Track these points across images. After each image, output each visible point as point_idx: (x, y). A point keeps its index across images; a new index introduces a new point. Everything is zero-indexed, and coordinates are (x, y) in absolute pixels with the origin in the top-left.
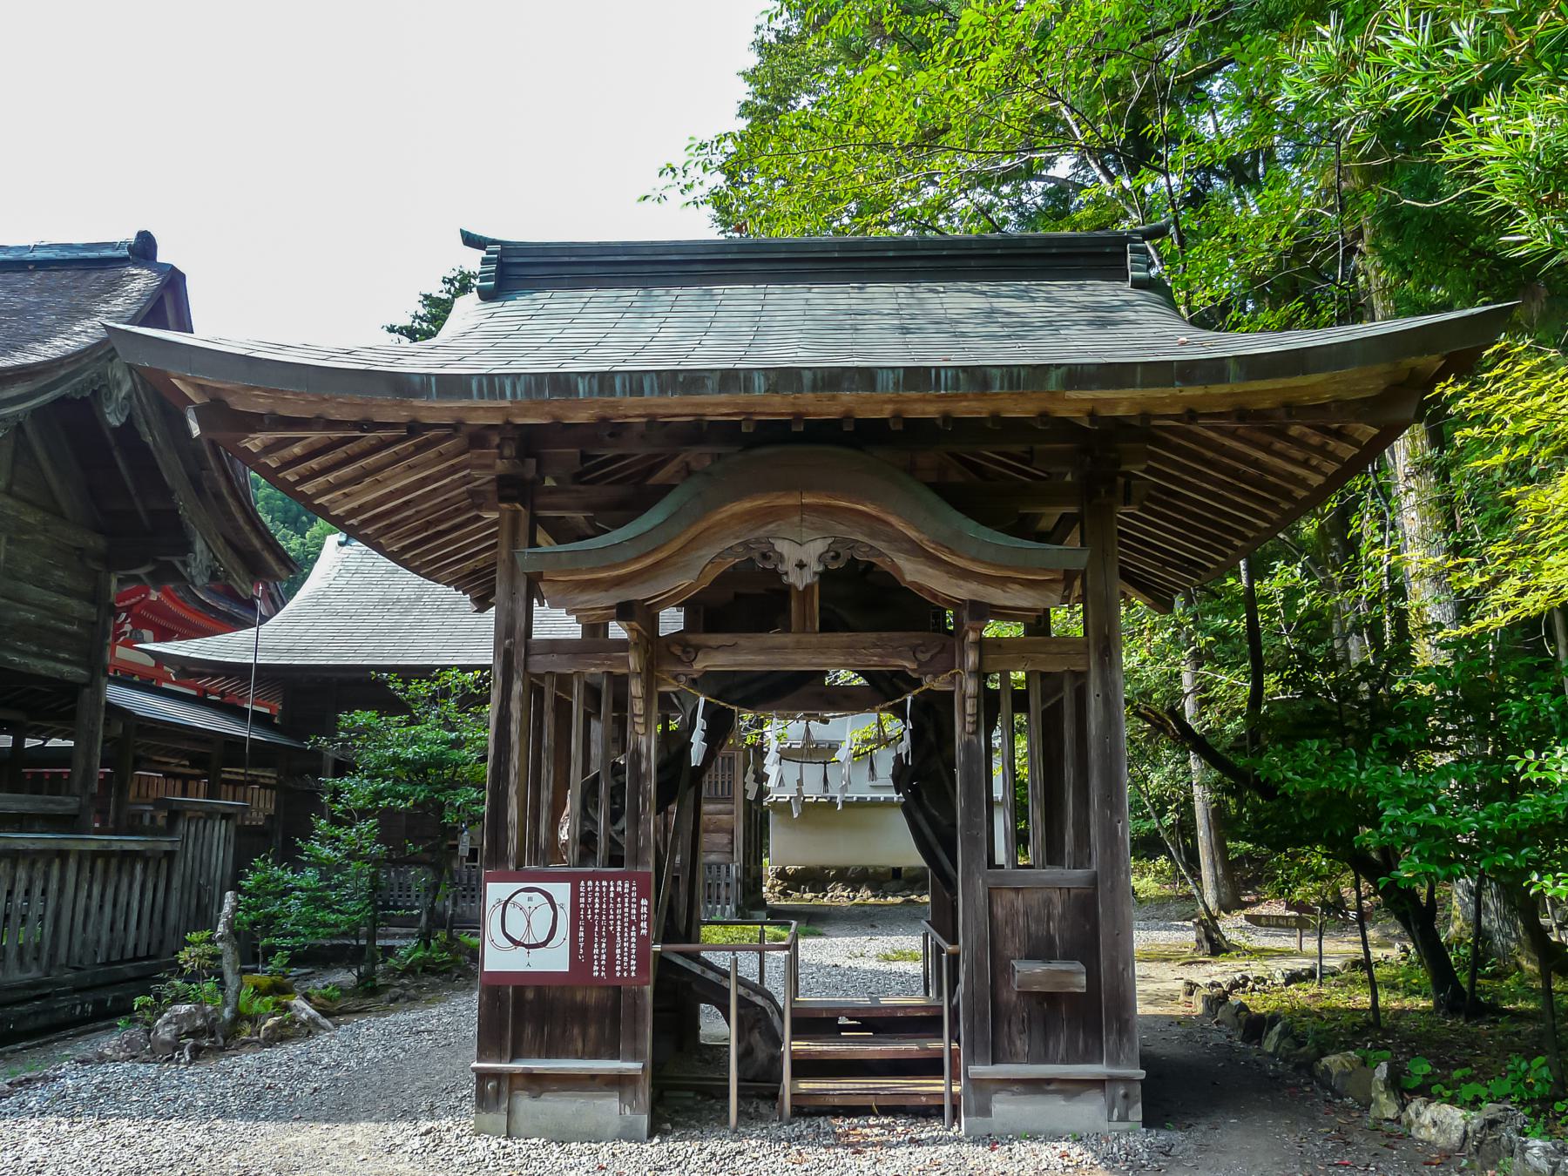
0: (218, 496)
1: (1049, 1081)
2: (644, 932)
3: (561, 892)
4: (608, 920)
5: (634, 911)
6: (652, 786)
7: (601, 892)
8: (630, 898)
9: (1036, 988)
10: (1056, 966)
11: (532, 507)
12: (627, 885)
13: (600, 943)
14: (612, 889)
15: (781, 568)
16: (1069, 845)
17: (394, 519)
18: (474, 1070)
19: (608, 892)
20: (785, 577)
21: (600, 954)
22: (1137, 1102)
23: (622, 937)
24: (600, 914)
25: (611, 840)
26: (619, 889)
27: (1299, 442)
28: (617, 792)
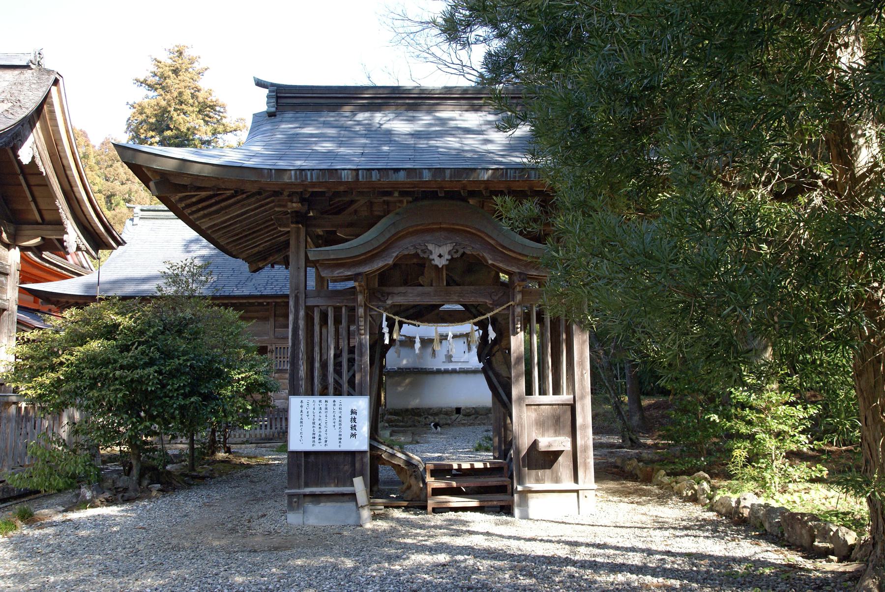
11: (307, 226)
15: (431, 257)
18: (286, 493)
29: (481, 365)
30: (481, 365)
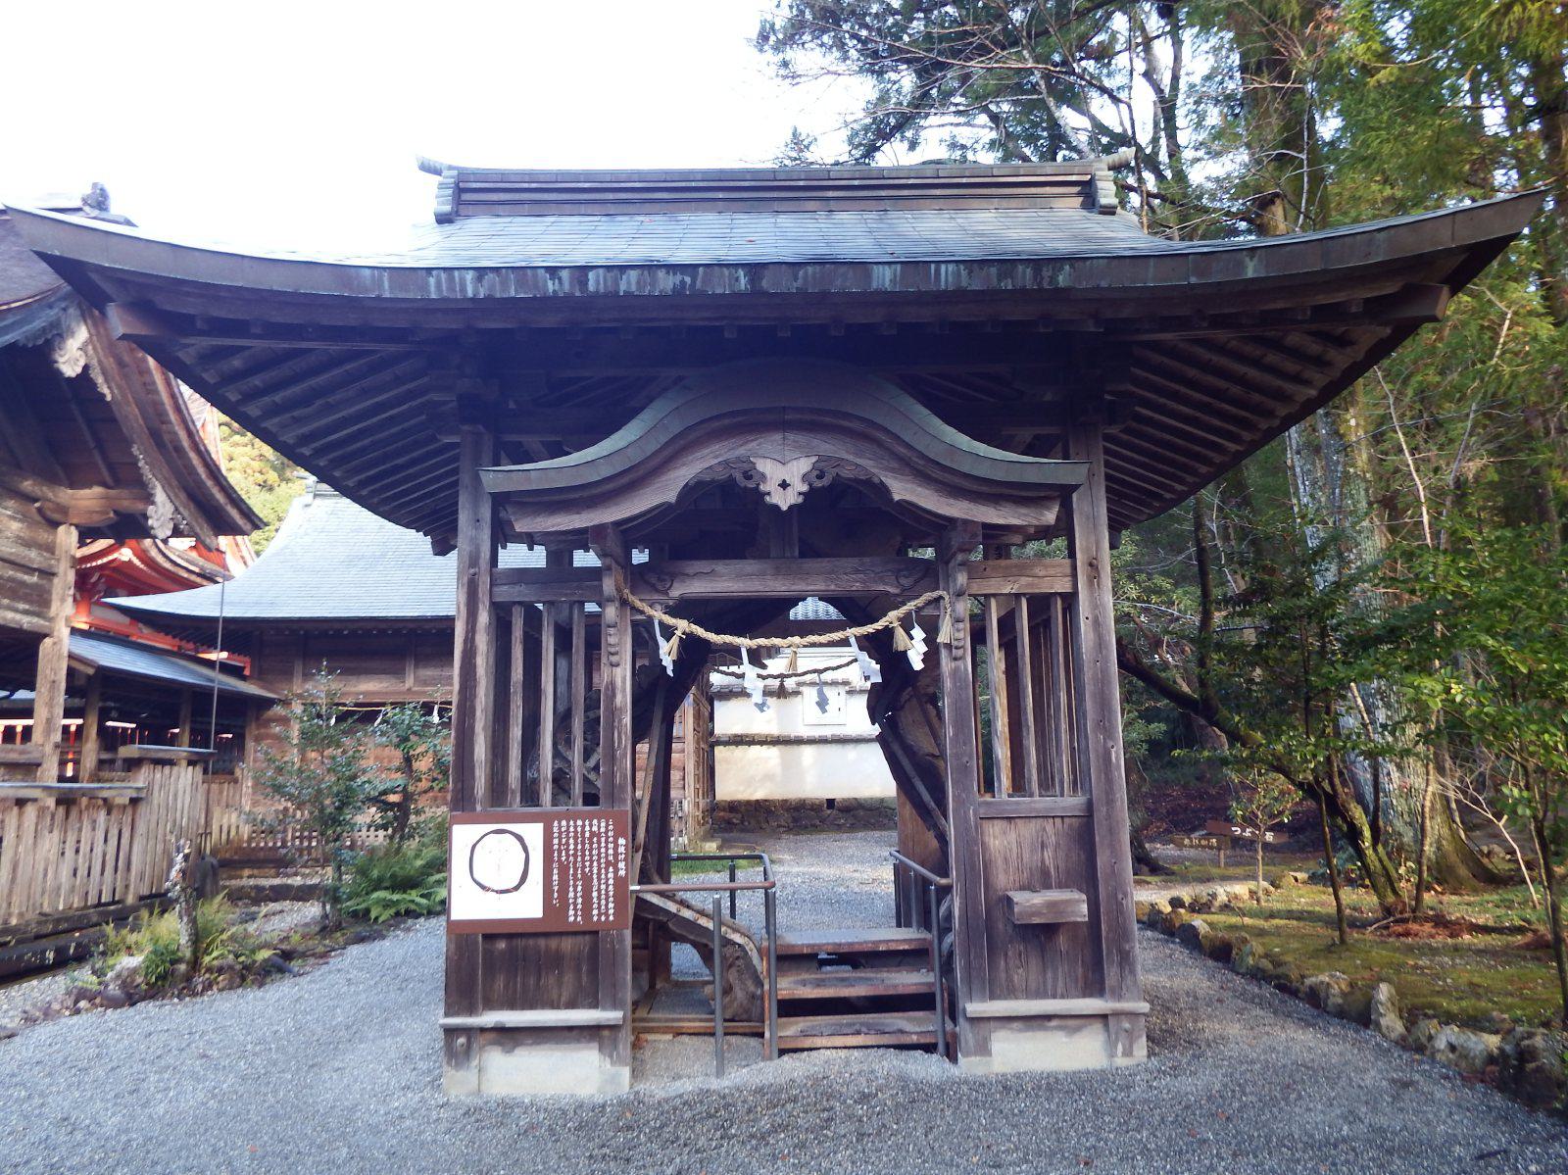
0: (179, 449)
1: (1049, 1017)
2: (622, 873)
3: (533, 833)
4: (583, 861)
5: (611, 852)
6: (627, 720)
7: (576, 832)
8: (607, 838)
9: (1036, 920)
10: (1055, 895)
12: (603, 824)
13: (575, 886)
14: (587, 828)
16: (1033, 773)
17: (350, 449)
19: (583, 832)
20: (768, 498)
21: (576, 898)
22: (1140, 1036)
23: (599, 879)
24: (575, 855)
25: (586, 780)
26: (595, 829)
27: (1296, 353)
28: (592, 726)
29: (876, 730)
30: (876, 730)
